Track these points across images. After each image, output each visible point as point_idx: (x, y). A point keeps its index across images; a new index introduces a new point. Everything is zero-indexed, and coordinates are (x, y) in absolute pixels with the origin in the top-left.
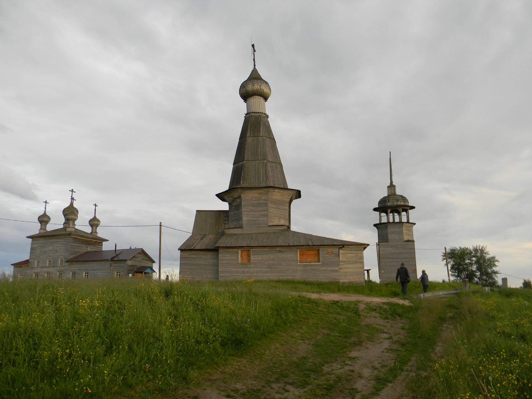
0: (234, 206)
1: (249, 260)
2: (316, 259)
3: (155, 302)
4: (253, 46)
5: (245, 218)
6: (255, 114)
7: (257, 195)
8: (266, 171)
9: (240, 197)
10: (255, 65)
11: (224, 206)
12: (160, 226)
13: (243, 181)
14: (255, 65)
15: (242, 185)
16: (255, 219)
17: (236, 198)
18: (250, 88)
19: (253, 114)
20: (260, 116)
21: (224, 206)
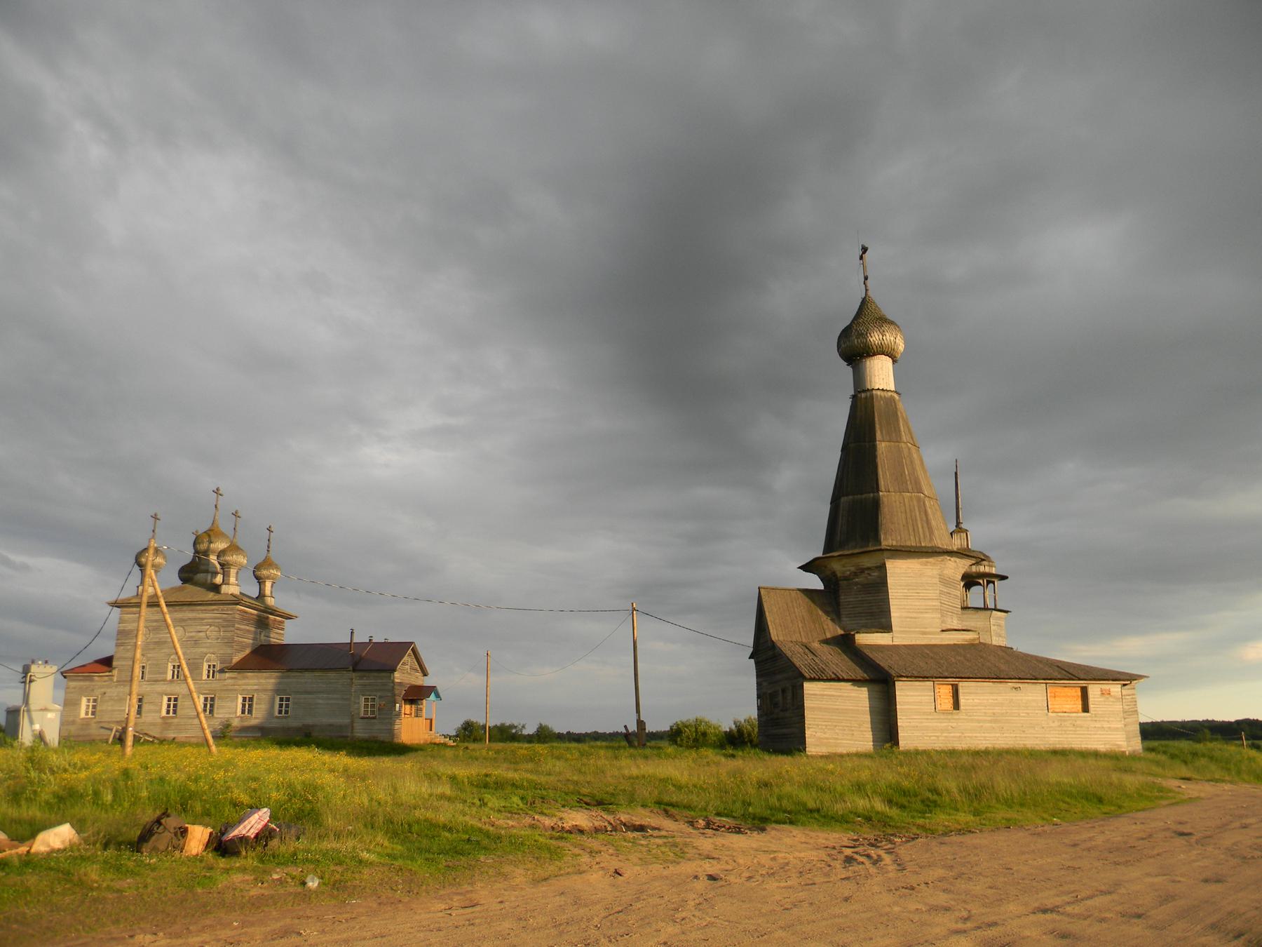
0: (857, 584)
1: (956, 705)
4: (865, 250)
7: (919, 566)
9: (882, 568)
17: (869, 569)
20: (872, 396)
21: (814, 582)
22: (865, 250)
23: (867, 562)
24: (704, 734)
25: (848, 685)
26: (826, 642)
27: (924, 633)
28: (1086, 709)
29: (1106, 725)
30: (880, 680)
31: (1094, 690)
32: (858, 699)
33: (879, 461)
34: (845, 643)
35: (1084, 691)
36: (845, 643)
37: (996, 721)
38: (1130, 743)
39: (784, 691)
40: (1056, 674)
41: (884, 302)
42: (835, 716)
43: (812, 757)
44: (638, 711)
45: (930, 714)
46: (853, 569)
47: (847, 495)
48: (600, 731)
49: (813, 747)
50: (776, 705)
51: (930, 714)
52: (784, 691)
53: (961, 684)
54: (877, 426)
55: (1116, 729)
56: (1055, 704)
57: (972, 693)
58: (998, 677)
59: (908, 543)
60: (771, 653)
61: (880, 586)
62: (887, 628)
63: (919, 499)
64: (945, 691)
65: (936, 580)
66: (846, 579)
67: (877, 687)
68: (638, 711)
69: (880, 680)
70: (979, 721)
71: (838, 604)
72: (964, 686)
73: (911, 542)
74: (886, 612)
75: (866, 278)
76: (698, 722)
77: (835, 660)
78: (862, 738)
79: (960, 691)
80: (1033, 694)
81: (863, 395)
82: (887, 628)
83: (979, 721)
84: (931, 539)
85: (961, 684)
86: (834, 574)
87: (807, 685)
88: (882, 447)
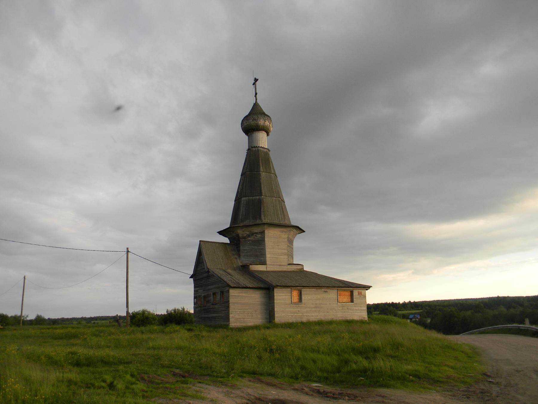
0: (249, 240)
1: (300, 299)
2: (349, 300)
3: (290, 345)
4: (256, 80)
5: (268, 256)
6: (263, 149)
7: (279, 233)
8: (282, 208)
9: (263, 233)
10: (256, 100)
11: (226, 240)
12: (128, 252)
13: (264, 216)
14: (256, 100)
15: (265, 221)
16: (276, 256)
17: (256, 233)
18: (251, 122)
19: (261, 149)
20: (258, 150)
21: (226, 240)
22: (256, 80)
23: (256, 230)
24: (147, 318)
25: (251, 291)
26: (234, 269)
27: (280, 265)
28: (352, 301)
29: (360, 308)
30: (267, 288)
31: (356, 293)
32: (255, 298)
33: (262, 181)
34: (245, 269)
35: (352, 293)
36: (245, 269)
37: (316, 307)
38: (364, 315)
39: (214, 294)
40: (341, 285)
41: (265, 107)
42: (244, 308)
43: (232, 329)
44: (127, 306)
45: (289, 304)
46: (248, 233)
47: (245, 197)
48: (66, 317)
49: (233, 323)
50: (208, 302)
51: (289, 304)
52: (214, 294)
53: (303, 290)
54: (261, 164)
55: (364, 310)
56: (340, 299)
57: (309, 296)
58: (318, 287)
59: (275, 222)
60: (205, 275)
61: (262, 241)
62: (264, 263)
63: (279, 201)
64: (295, 293)
65: (286, 240)
66: (244, 238)
67: (264, 292)
68: (127, 306)
69: (267, 288)
70: (309, 308)
71: (239, 251)
72: (305, 291)
73: (276, 222)
74: (263, 255)
75: (256, 94)
76: (144, 312)
77: (243, 280)
78: (255, 318)
79: (303, 293)
80: (332, 294)
81: (254, 149)
82: (264, 263)
83: (309, 308)
84: (284, 220)
85: (303, 290)
86: (238, 235)
87: (232, 292)
88: (263, 175)
